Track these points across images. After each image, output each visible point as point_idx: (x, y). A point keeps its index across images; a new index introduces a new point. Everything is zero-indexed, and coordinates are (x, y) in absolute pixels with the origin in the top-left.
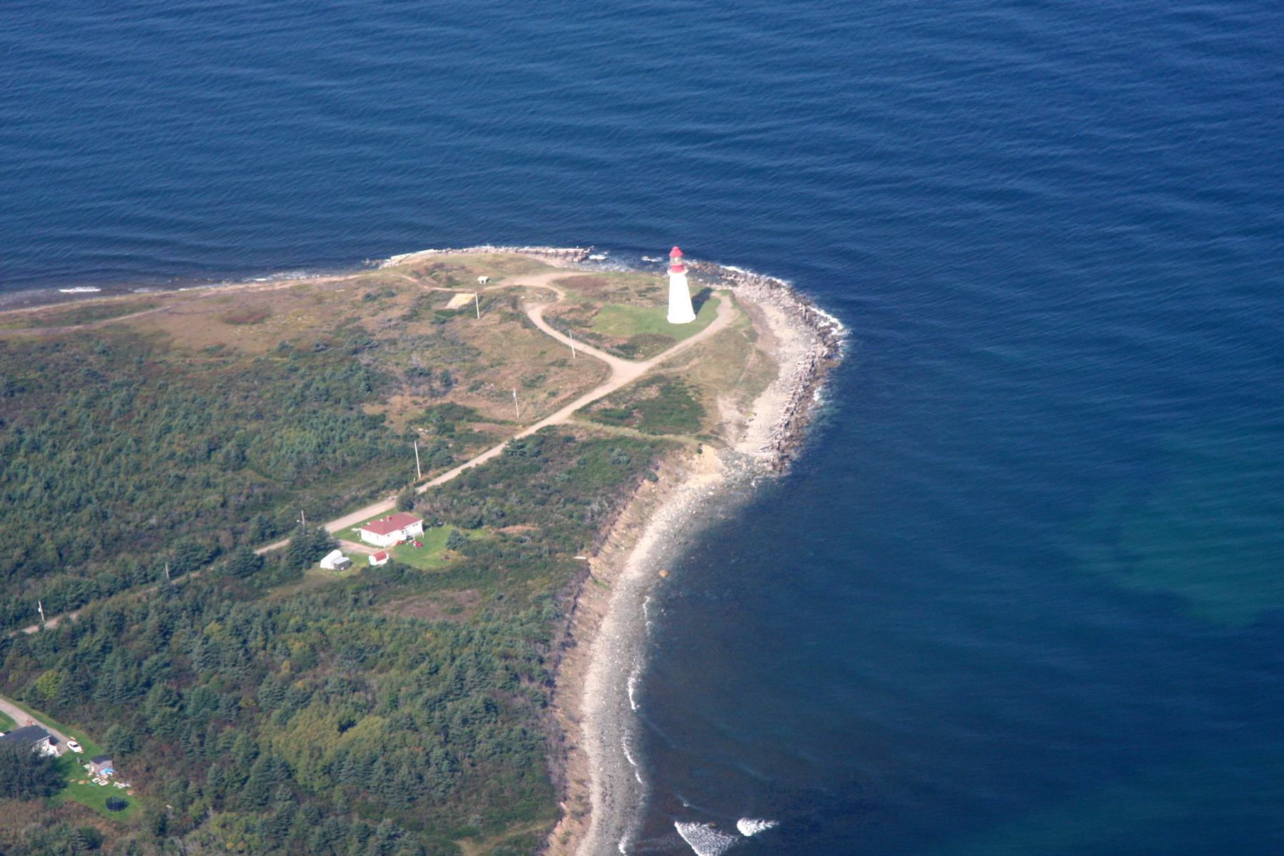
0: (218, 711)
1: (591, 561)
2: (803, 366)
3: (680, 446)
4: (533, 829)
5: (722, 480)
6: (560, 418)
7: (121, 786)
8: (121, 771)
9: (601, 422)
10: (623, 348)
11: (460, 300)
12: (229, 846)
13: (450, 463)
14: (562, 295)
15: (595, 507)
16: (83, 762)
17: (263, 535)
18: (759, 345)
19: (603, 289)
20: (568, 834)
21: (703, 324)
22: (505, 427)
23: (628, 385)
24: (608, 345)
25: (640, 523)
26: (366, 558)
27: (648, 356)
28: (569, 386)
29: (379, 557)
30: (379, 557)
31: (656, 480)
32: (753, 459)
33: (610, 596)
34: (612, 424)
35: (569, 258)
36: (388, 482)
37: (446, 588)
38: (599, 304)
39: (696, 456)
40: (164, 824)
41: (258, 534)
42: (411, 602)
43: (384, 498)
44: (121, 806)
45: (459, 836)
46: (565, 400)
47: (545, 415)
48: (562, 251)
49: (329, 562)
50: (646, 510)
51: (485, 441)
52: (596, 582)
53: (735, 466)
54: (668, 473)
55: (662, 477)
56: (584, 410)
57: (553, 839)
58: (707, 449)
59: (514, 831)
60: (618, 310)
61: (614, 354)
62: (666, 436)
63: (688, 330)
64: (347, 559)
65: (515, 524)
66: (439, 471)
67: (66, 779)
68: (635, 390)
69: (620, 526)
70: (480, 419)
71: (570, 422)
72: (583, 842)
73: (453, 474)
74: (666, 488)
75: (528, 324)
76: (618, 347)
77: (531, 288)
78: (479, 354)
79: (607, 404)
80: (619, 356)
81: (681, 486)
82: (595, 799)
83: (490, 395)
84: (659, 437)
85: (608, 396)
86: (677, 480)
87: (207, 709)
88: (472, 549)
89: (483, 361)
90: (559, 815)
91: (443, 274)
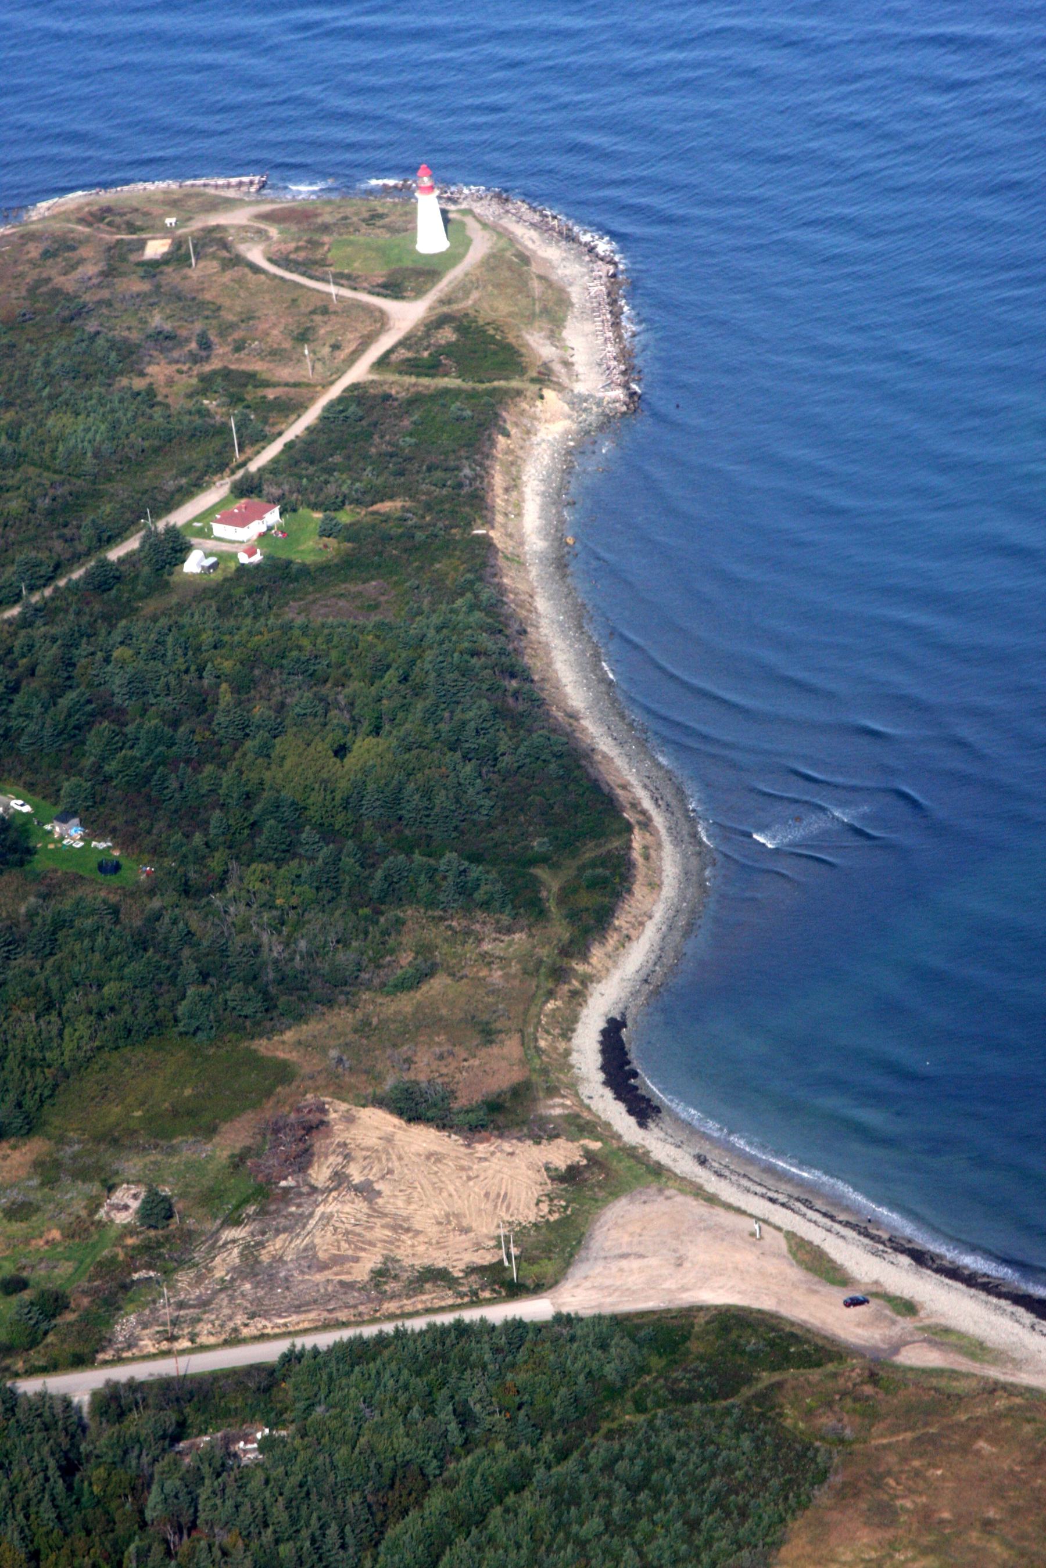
0: (174, 748)
1: (492, 534)
2: (599, 288)
3: (519, 393)
4: (609, 846)
5: (574, 427)
6: (359, 372)
7: (102, 845)
8: (94, 828)
9: (411, 374)
10: (384, 286)
11: (156, 248)
12: (279, 902)
13: (267, 439)
14: (273, 232)
15: (467, 471)
16: (41, 824)
17: (100, 540)
18: (534, 268)
19: (319, 220)
20: (646, 848)
21: (461, 250)
22: (304, 390)
23: (416, 327)
24: (365, 285)
25: (514, 485)
26: (234, 556)
27: (419, 293)
28: (350, 336)
29: (251, 553)
30: (251, 553)
31: (508, 435)
32: (602, 399)
33: (528, 572)
34: (427, 375)
35: (244, 189)
36: (209, 466)
37: (344, 582)
38: (326, 239)
39: (538, 403)
40: (186, 883)
41: (95, 539)
42: (314, 602)
43: (209, 485)
44: (116, 868)
45: (533, 862)
46: (354, 352)
47: (340, 372)
48: (234, 181)
49: (194, 564)
50: (514, 469)
51: (292, 408)
52: (507, 559)
53: (585, 410)
54: (516, 425)
55: (513, 431)
56: (382, 363)
57: (636, 855)
58: (548, 393)
59: (589, 852)
60: (351, 243)
61: (378, 294)
62: (496, 383)
63: (450, 259)
64: (212, 560)
65: (382, 501)
66: (257, 448)
67: (31, 845)
68: (427, 335)
69: (499, 490)
70: (267, 384)
71: (372, 377)
72: (663, 854)
73: (273, 450)
74: (521, 442)
75: (256, 269)
76: (378, 286)
77: (233, 226)
78: (219, 308)
79: (403, 353)
80: (385, 296)
81: (535, 439)
82: (647, 804)
83: (261, 355)
84: (488, 385)
85: (401, 344)
86: (528, 432)
87: (161, 748)
88: (351, 534)
89: (231, 318)
90: (629, 828)
91: (118, 220)
